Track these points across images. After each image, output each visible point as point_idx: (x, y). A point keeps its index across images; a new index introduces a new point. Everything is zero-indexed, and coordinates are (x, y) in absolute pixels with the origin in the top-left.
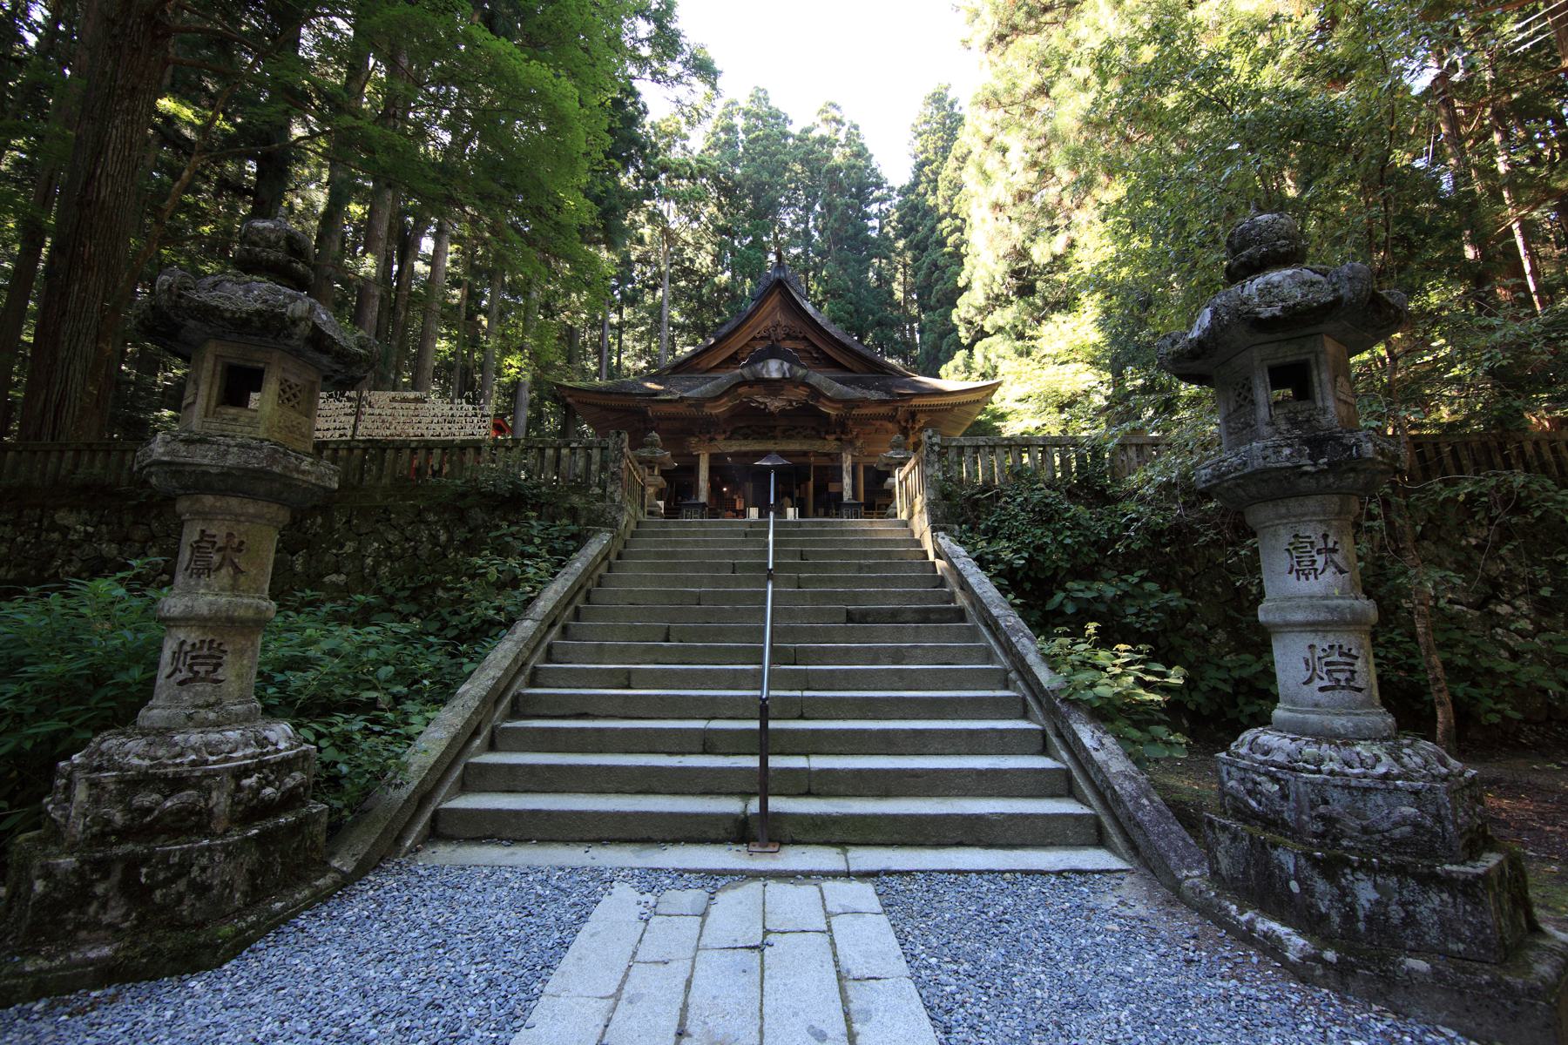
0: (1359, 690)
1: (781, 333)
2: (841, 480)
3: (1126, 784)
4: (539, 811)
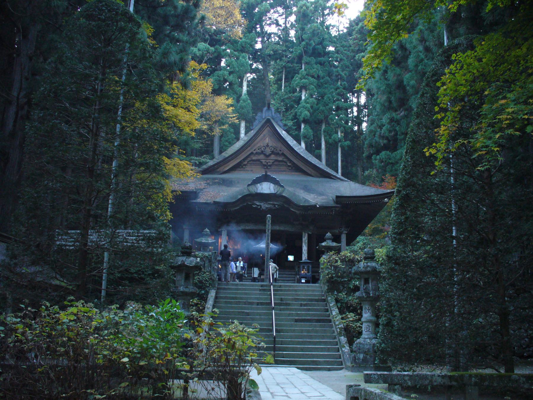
1: (268, 151)
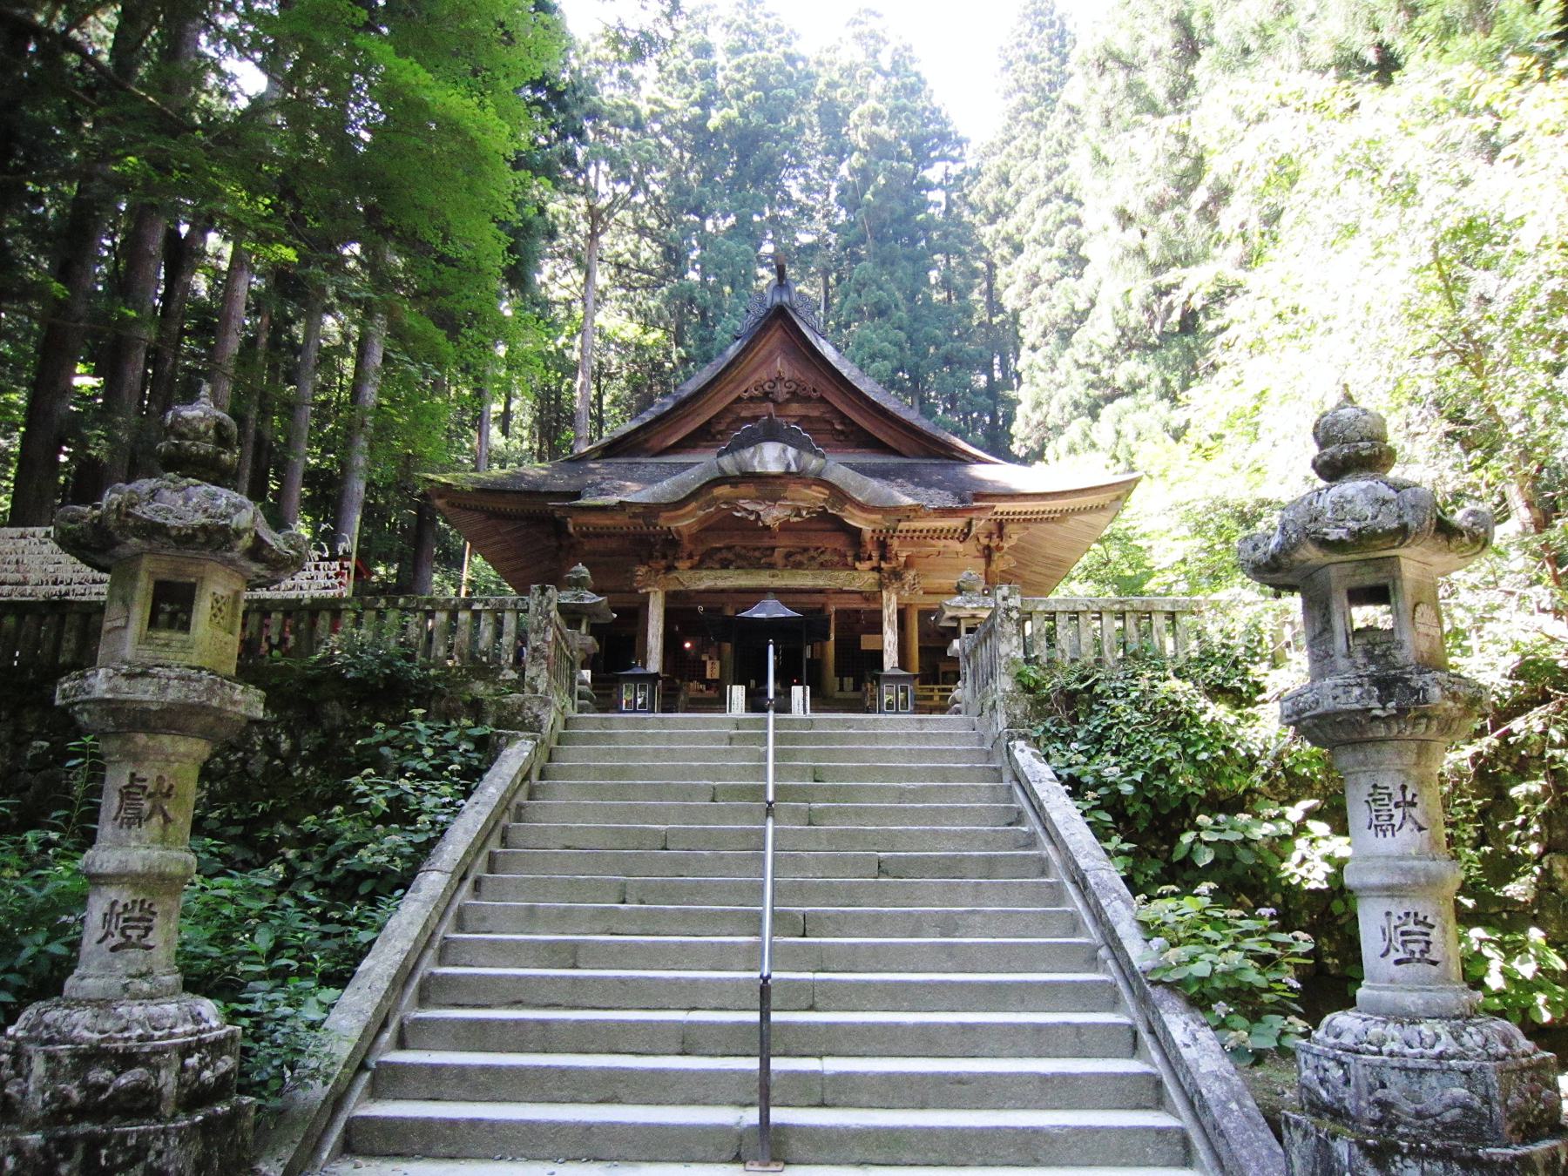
0: (1434, 963)
1: (782, 392)
2: (880, 631)
3: (1216, 1086)
4: (480, 1120)
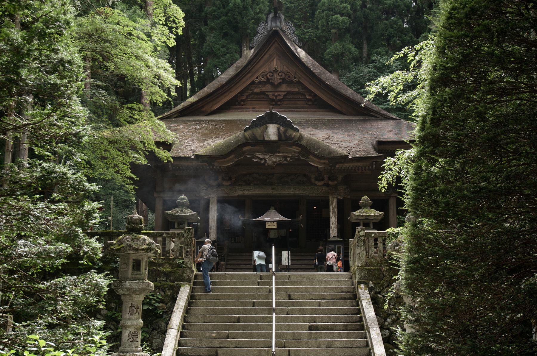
1: (277, 79)
